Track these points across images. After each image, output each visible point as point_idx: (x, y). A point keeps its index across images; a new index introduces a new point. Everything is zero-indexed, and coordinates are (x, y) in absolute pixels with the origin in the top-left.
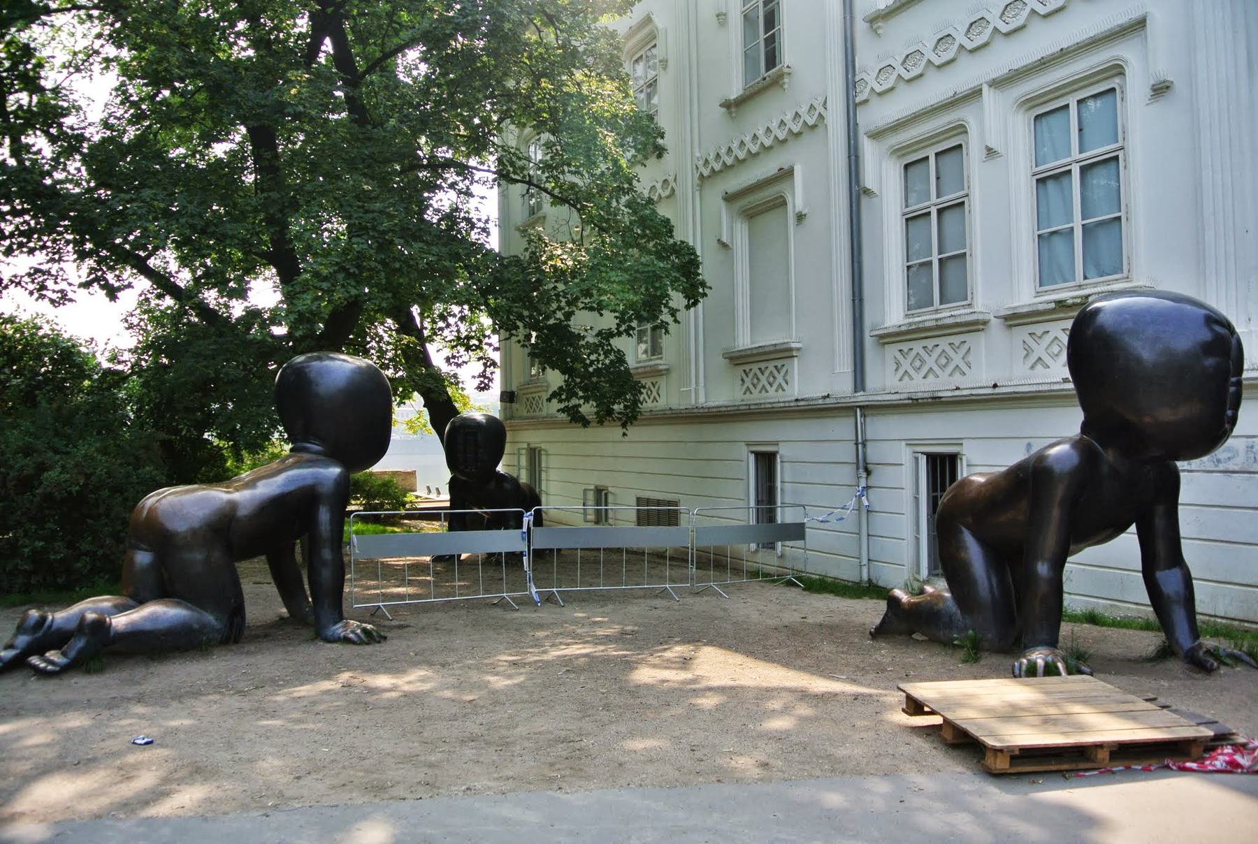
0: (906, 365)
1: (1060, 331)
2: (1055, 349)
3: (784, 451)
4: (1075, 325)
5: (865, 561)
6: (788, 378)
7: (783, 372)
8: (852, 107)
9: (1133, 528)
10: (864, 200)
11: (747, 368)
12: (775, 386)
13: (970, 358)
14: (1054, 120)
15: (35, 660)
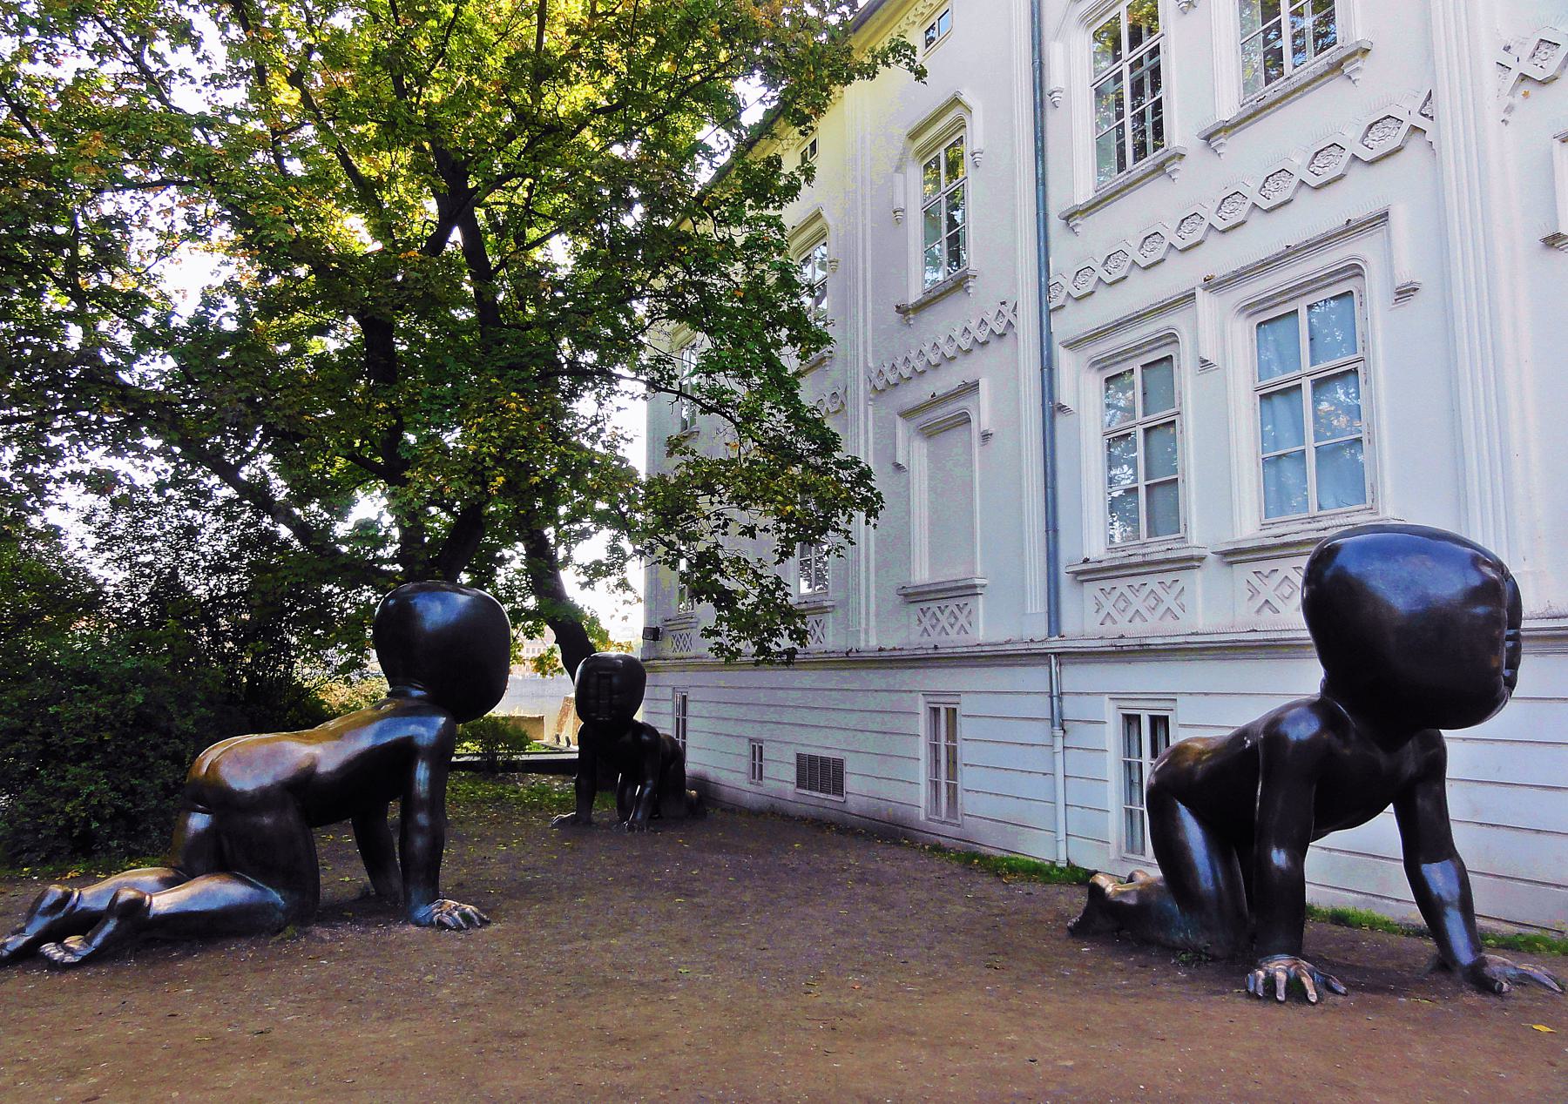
0: (1108, 607)
1: (1294, 570)
2: (1286, 590)
3: (965, 706)
4: (1313, 563)
5: (1062, 836)
7: (965, 612)
8: (1046, 313)
9: (1391, 807)
10: (1060, 419)
11: (925, 606)
12: (956, 627)
13: (1184, 599)
14: (1281, 327)
15: (50, 949)
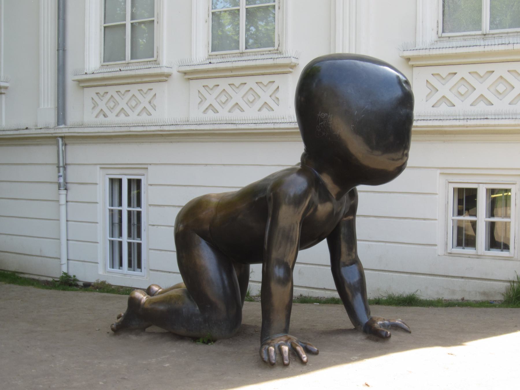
0: (102, 105)
6: (155, 102)
9: (325, 240)
